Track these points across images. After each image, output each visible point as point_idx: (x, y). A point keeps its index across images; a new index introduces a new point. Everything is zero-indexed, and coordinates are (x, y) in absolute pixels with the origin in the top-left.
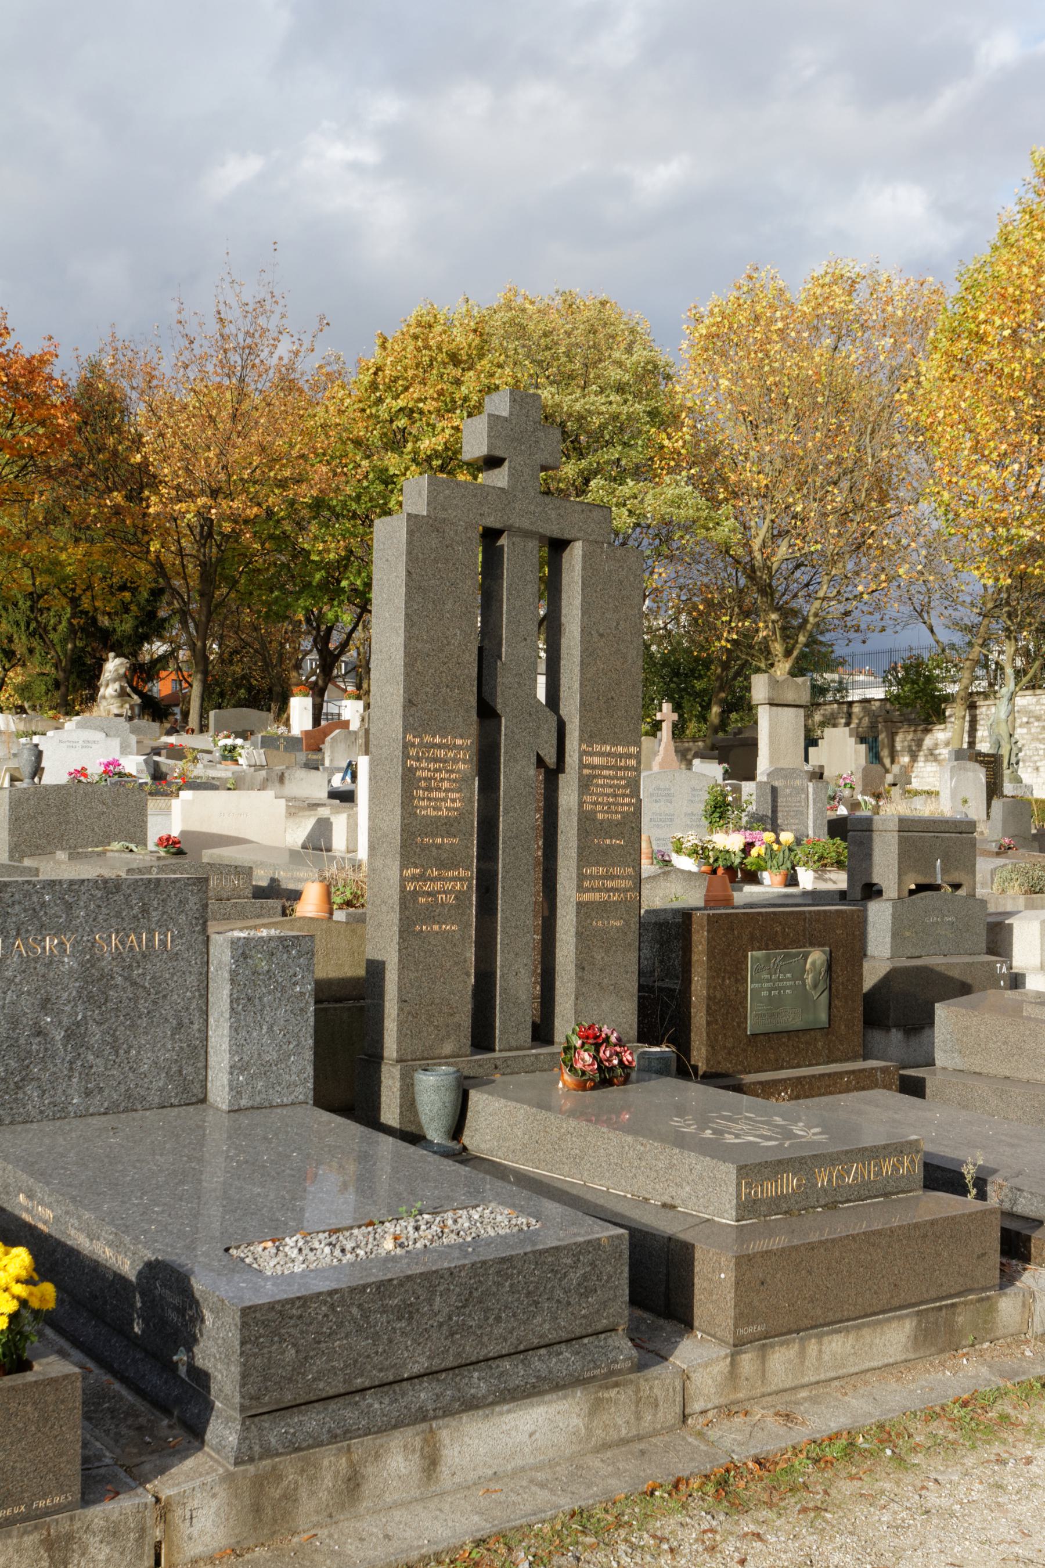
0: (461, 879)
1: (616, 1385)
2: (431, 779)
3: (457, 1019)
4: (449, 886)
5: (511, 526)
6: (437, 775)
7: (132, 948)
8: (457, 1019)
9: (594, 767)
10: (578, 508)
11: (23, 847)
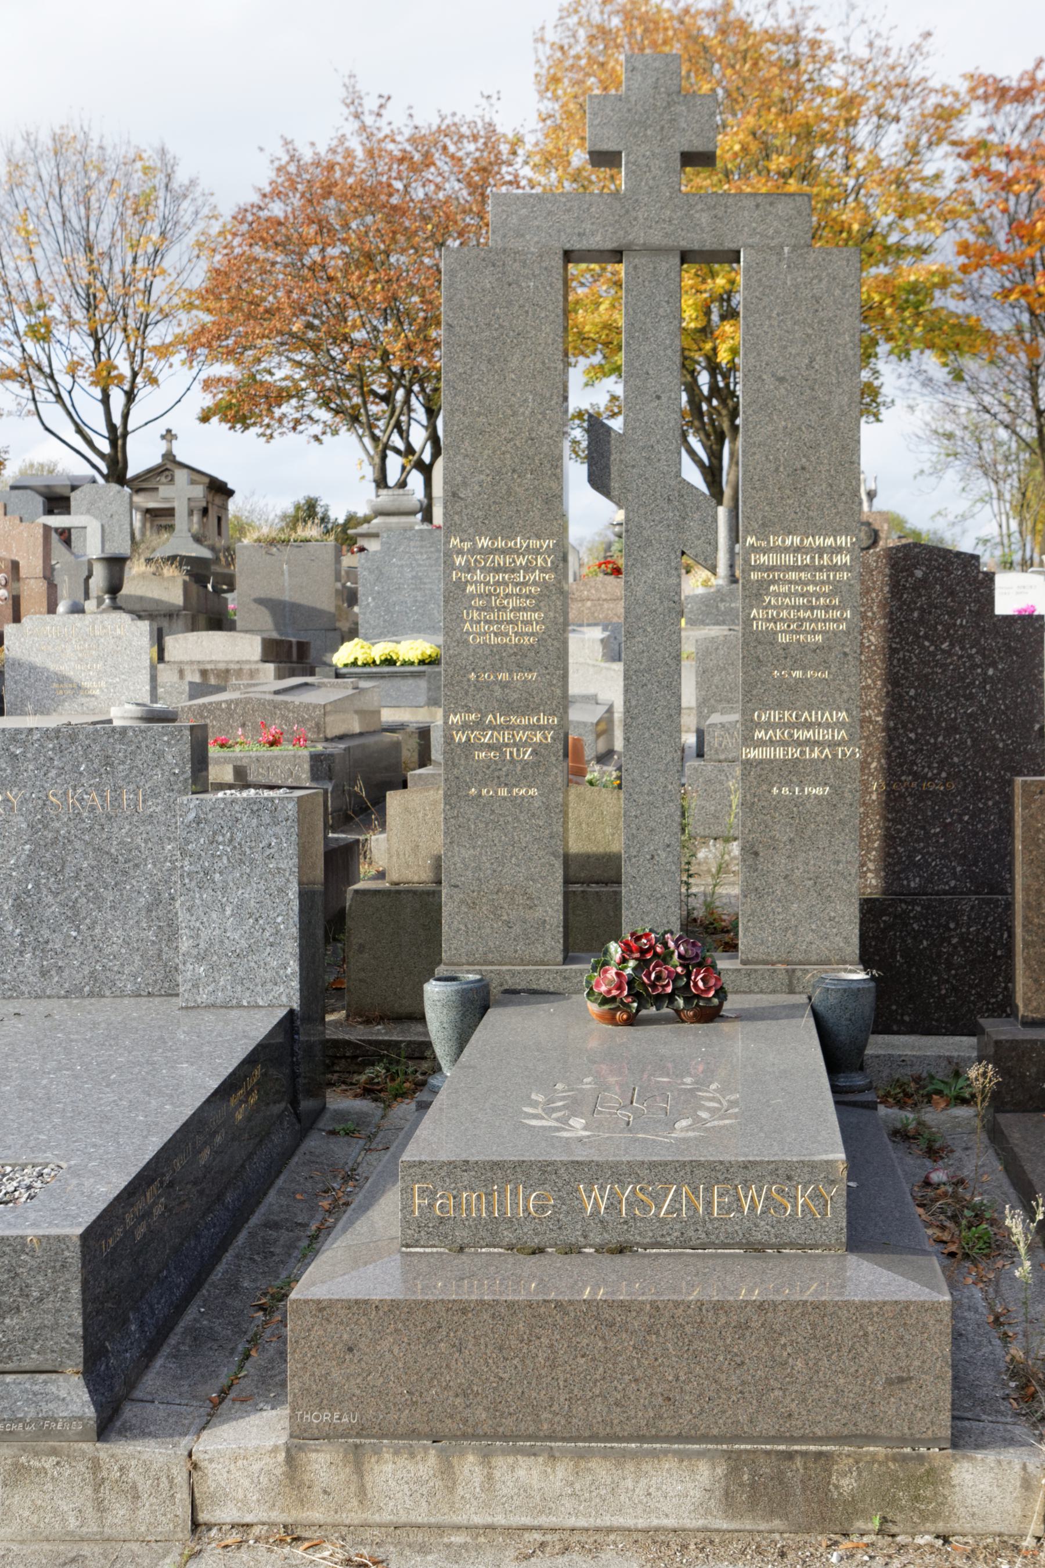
0: (541, 728)
1: (54, 1452)
2: (490, 595)
3: (539, 912)
4: (521, 736)
5: (631, 243)
6: (500, 590)
7: (93, 809)
8: (539, 912)
9: (770, 569)
10: (750, 203)
11: (712, 701)
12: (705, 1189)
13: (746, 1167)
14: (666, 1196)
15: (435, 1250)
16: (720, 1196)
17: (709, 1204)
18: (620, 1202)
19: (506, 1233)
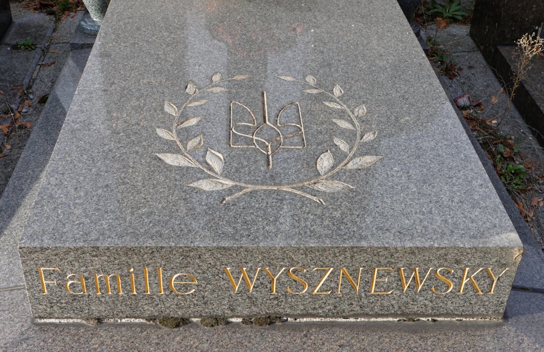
12: (366, 272)
13: (413, 253)
14: (321, 277)
15: (71, 321)
16: (379, 277)
17: (368, 283)
18: (271, 282)
19: (146, 307)
